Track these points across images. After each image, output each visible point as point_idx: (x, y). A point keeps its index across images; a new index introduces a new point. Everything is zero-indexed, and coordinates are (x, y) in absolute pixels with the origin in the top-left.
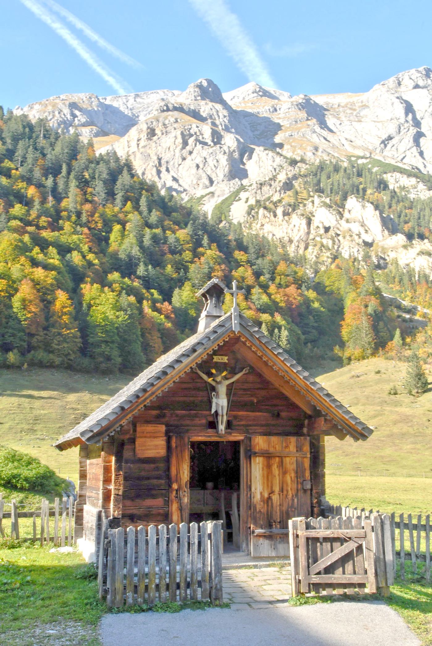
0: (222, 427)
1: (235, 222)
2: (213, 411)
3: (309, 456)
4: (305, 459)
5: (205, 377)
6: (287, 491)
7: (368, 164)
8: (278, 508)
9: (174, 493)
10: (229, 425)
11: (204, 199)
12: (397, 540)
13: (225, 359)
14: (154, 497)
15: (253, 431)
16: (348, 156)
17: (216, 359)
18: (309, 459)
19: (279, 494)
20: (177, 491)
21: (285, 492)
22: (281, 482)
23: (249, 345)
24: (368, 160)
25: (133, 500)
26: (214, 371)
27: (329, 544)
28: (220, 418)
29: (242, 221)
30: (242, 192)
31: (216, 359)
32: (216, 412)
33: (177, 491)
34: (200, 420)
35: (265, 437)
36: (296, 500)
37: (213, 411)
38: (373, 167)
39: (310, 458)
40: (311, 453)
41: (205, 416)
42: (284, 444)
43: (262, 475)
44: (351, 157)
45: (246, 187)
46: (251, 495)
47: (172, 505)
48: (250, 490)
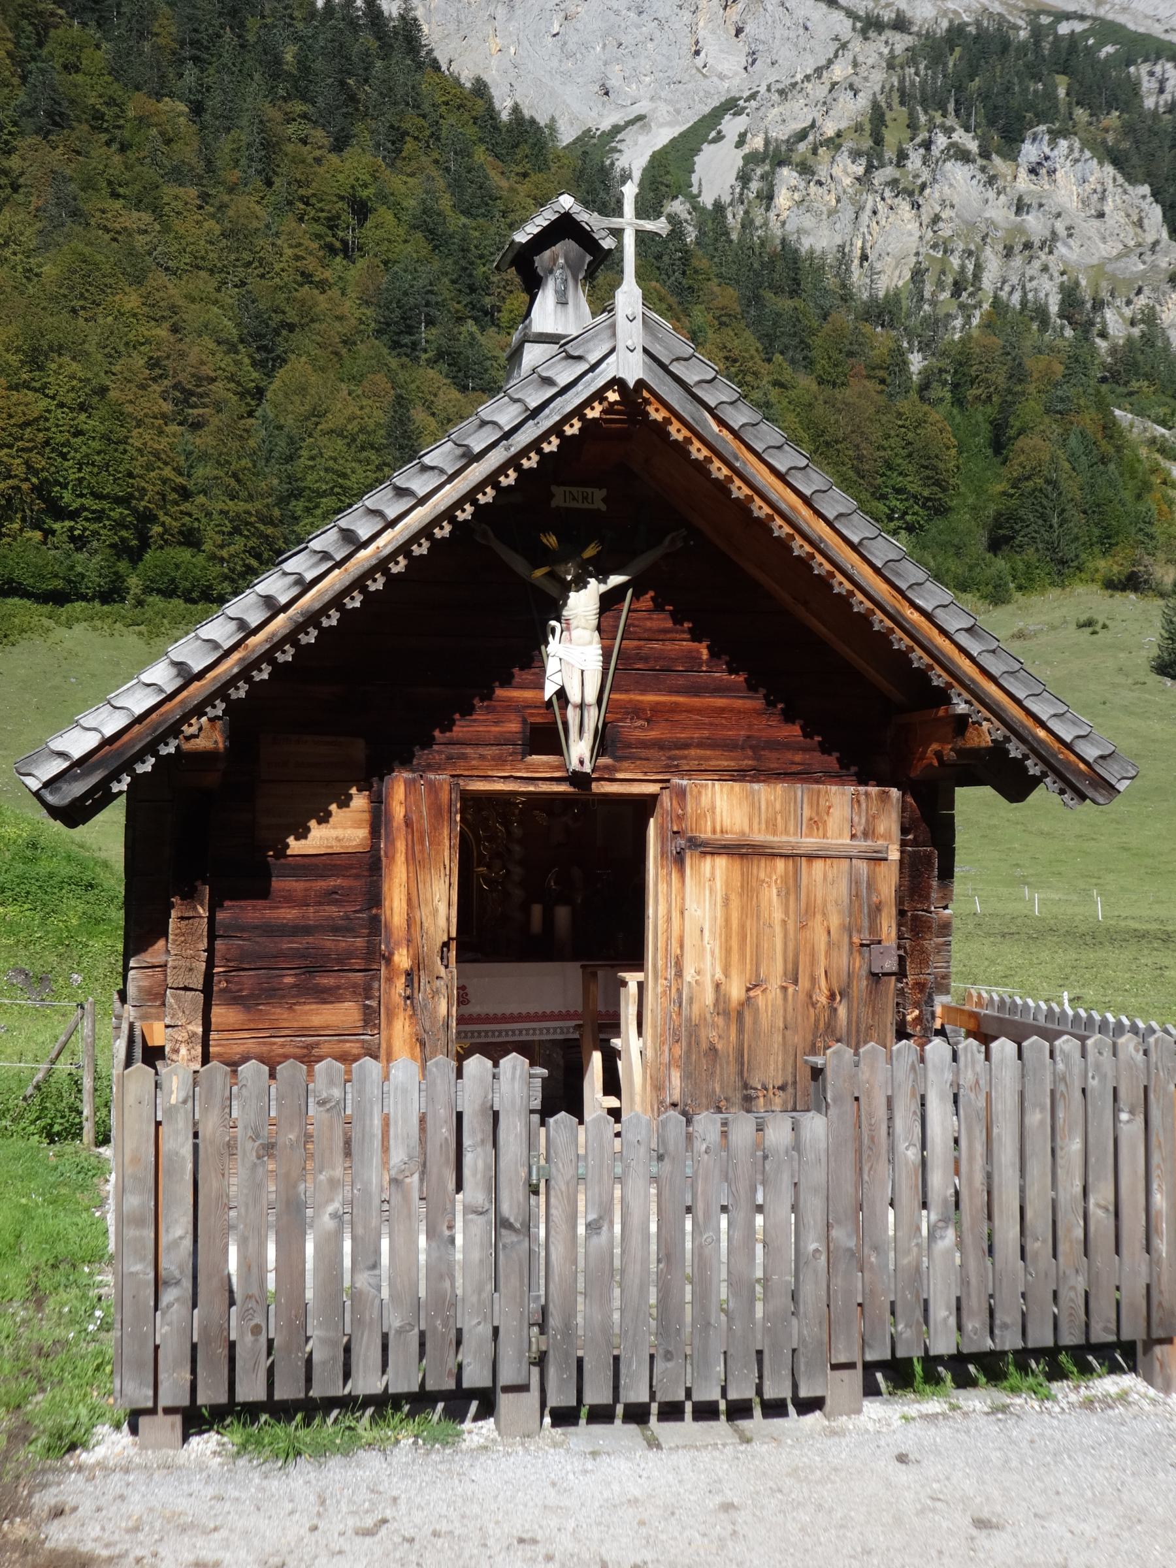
0: (579, 751)
1: (707, 200)
2: (550, 690)
3: (894, 855)
4: (883, 868)
5: (518, 564)
6: (813, 980)
7: (1085, 34)
8: (778, 1038)
9: (400, 983)
10: (604, 742)
11: (619, 137)
12: (507, 449)
13: (597, 498)
14: (325, 996)
15: (694, 764)
16: (1029, 12)
17: (561, 497)
18: (895, 869)
19: (784, 989)
20: (409, 974)
21: (804, 982)
22: (790, 966)
23: (680, 437)
24: (1085, 25)
25: (248, 1009)
26: (551, 541)
27: (895, 968)
28: (572, 715)
29: (726, 199)
30: (727, 117)
31: (561, 497)
32: (561, 694)
33: (409, 974)
34: (497, 723)
35: (737, 786)
36: (842, 1011)
37: (550, 690)
38: (1101, 44)
39: (901, 861)
40: (903, 844)
41: (520, 708)
42: (807, 813)
43: (720, 921)
44: (1038, 14)
45: (741, 102)
46: (680, 992)
47: (390, 1023)
48: (679, 974)
